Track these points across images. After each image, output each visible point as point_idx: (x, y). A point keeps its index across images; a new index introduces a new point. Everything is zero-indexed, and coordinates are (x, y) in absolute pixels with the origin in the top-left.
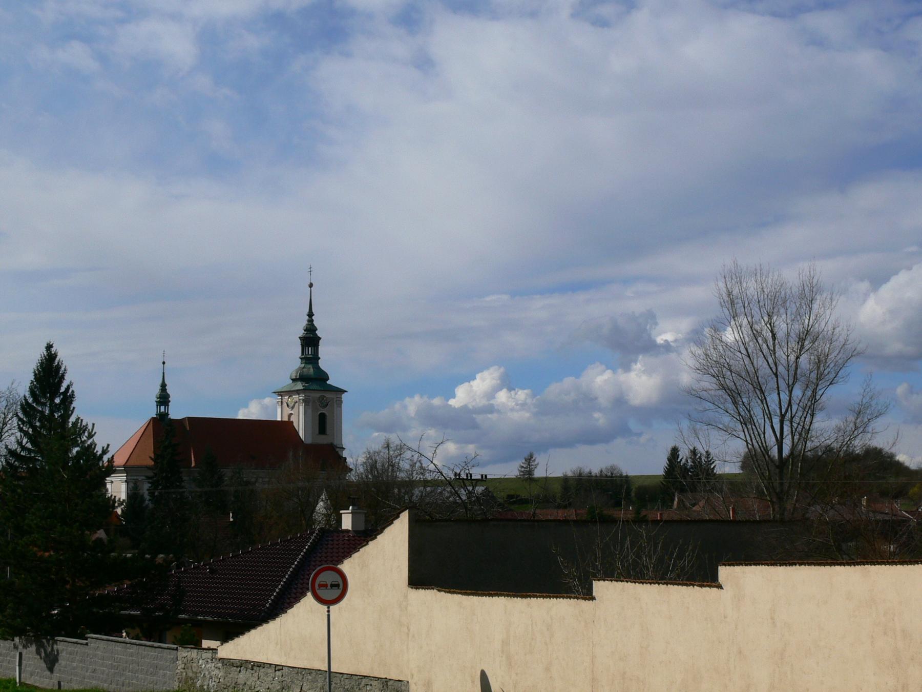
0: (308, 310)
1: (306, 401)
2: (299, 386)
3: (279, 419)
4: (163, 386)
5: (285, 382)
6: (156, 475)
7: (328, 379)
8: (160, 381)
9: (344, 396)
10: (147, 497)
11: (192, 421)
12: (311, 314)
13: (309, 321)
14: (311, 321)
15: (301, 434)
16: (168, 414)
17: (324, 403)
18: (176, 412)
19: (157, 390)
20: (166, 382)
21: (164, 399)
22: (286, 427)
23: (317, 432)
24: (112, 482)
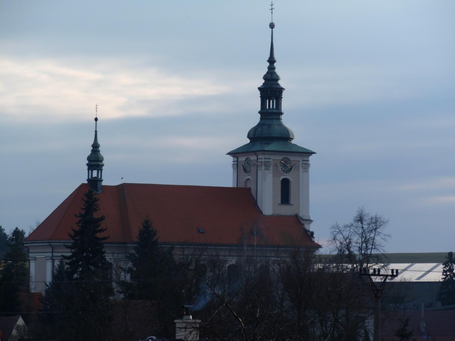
0: (268, 56)
4: (96, 147)
6: (74, 254)
9: (312, 158)
10: (255, 239)
11: (105, 186)
12: (272, 61)
14: (271, 69)
17: (287, 167)
18: (110, 179)
19: (88, 151)
20: (99, 141)
21: (95, 161)
24: (35, 259)
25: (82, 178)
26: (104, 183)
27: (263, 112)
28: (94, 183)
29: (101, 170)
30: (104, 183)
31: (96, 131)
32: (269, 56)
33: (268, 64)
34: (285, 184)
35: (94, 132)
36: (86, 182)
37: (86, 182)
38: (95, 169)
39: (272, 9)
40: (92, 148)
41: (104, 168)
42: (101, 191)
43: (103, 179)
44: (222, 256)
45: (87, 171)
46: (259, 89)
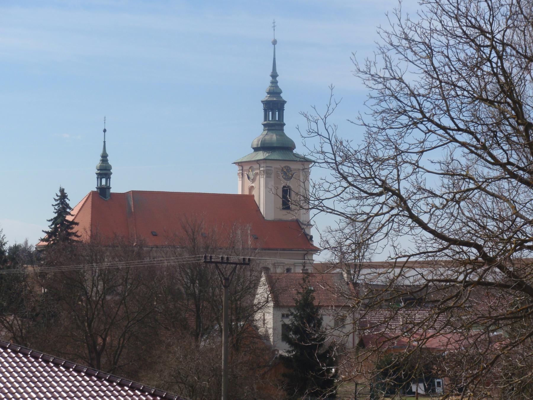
0: (271, 70)
1: (268, 174)
2: (261, 155)
3: (240, 193)
4: (104, 157)
5: (246, 153)
7: (294, 147)
8: (101, 152)
12: (274, 75)
13: (272, 82)
14: (274, 82)
15: (262, 210)
16: (109, 188)
17: (287, 174)
18: (119, 185)
19: (97, 161)
21: (104, 172)
22: (246, 202)
23: (280, 205)
25: (92, 185)
26: (112, 191)
28: (102, 192)
29: (110, 178)
30: (112, 191)
31: (104, 142)
32: (271, 71)
33: (271, 78)
34: (286, 191)
36: (96, 190)
37: (96, 190)
41: (112, 176)
42: (109, 198)
43: (111, 186)
46: (262, 102)
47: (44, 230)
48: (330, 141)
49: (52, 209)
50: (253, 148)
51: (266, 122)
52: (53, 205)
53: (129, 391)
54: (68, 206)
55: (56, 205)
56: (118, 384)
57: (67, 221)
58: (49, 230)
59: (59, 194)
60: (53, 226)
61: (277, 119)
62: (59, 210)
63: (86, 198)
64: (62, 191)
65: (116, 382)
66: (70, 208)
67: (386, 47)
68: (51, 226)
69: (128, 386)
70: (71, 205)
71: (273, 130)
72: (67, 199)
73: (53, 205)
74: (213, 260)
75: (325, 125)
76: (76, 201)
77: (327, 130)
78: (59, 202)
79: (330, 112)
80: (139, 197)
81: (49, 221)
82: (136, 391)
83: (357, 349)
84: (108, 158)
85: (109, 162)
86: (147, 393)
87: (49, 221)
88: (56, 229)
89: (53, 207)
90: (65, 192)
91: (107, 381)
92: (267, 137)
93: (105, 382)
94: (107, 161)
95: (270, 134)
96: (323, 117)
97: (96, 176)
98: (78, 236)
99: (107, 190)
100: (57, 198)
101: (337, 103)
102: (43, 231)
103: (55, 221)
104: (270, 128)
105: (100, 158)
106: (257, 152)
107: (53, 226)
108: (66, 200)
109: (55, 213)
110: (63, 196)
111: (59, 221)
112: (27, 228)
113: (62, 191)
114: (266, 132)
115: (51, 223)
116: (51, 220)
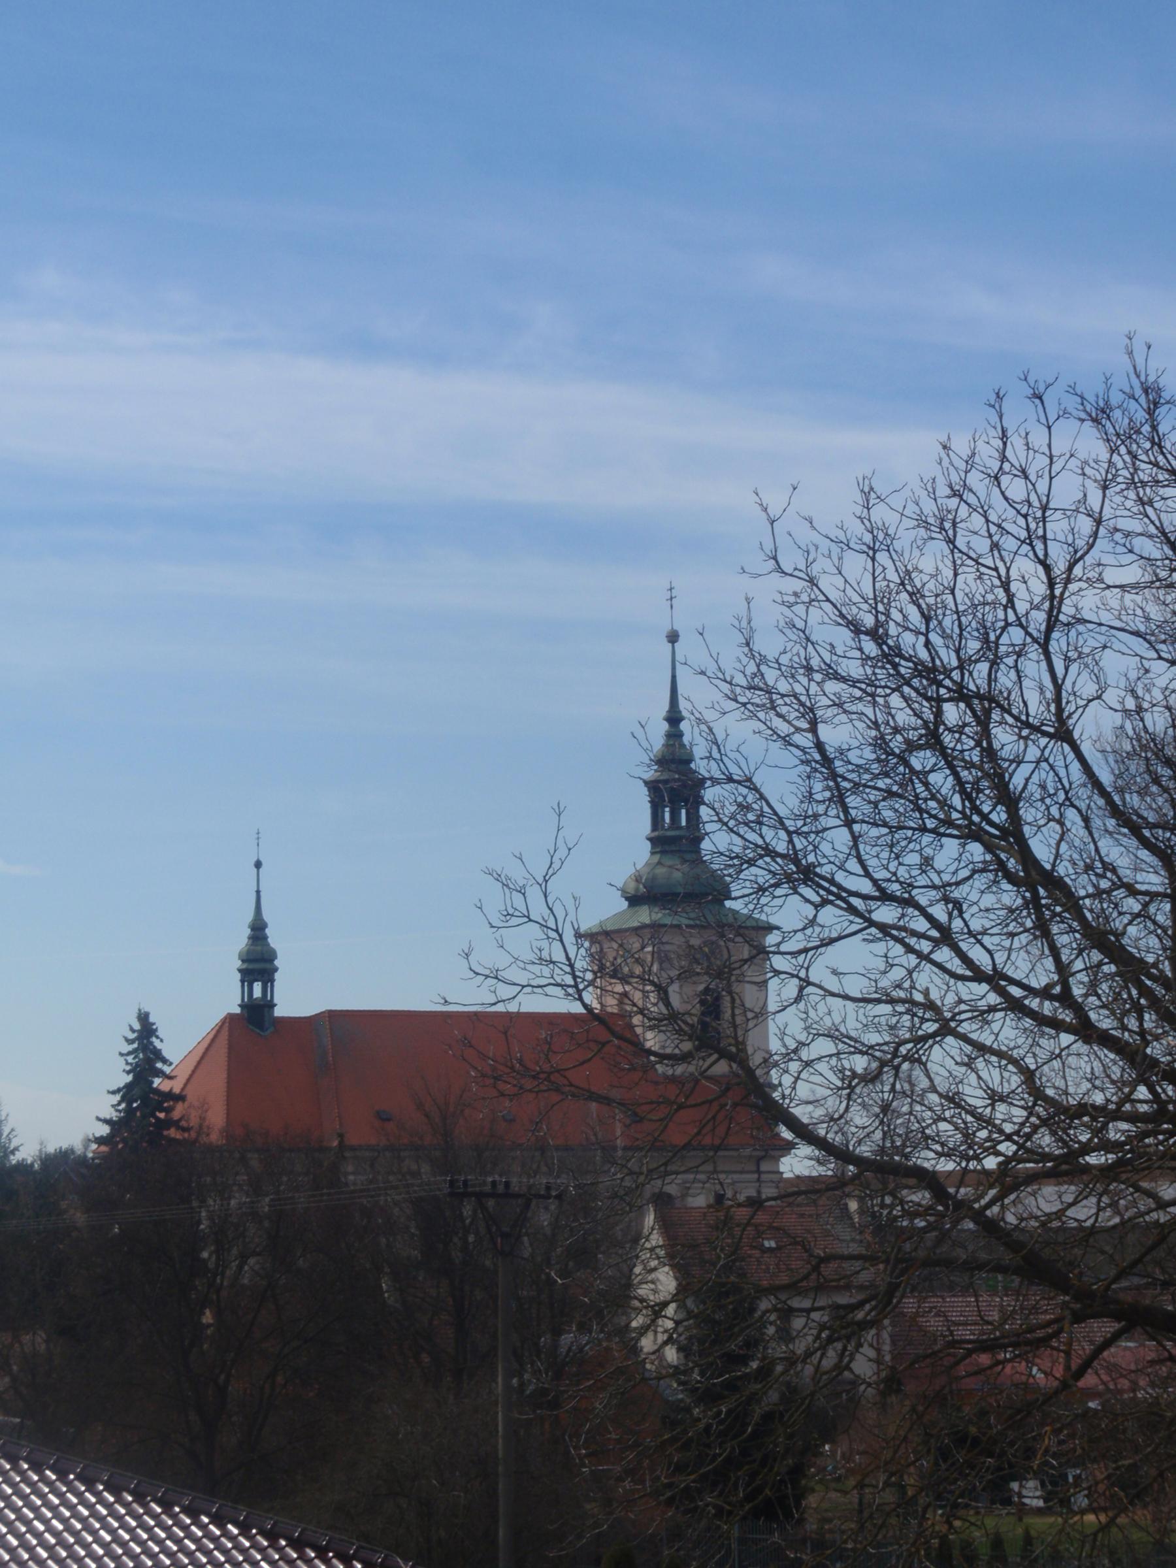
0: (665, 706)
2: (644, 915)
4: (258, 929)
14: (674, 735)
16: (271, 1006)
18: (294, 998)
19: (241, 939)
20: (267, 916)
21: (258, 964)
25: (229, 999)
26: (279, 1012)
27: (661, 842)
28: (256, 1015)
29: (272, 981)
30: (279, 1012)
31: (258, 892)
32: (667, 707)
33: (665, 726)
35: (254, 894)
36: (238, 1010)
37: (238, 1010)
38: (257, 980)
39: (671, 599)
40: (248, 931)
41: (277, 976)
42: (272, 1029)
43: (275, 1001)
44: (586, 1344)
45: (239, 984)
47: (102, 1116)
48: (560, 936)
49: (121, 1064)
50: (627, 899)
51: (656, 833)
52: (121, 1054)
53: (211, 1527)
54: (158, 1055)
55: (129, 1053)
56: (185, 1510)
57: (157, 1091)
58: (112, 1114)
59: (137, 1026)
60: (123, 1106)
61: (684, 823)
62: (137, 1065)
63: (213, 1033)
64: (143, 1018)
65: (179, 1506)
66: (165, 1061)
67: (716, 706)
68: (119, 1104)
69: (207, 1515)
70: (165, 1054)
71: (672, 852)
72: (157, 1037)
73: (121, 1054)
74: (470, 1190)
75: (546, 897)
76: (179, 1044)
77: (551, 909)
78: (135, 1045)
79: (556, 866)
80: (340, 1025)
81: (113, 1093)
82: (230, 1526)
83: (883, 1394)
84: (267, 931)
85: (269, 940)
86: (254, 1531)
87: (113, 1093)
88: (129, 1111)
89: (122, 1059)
90: (152, 1019)
91: (159, 1502)
92: (661, 871)
93: (153, 1505)
94: (265, 938)
95: (668, 861)
96: (541, 880)
97: (238, 976)
98: (184, 1130)
99: (266, 1009)
100: (132, 1036)
101: (570, 846)
102: (98, 1119)
103: (126, 1093)
104: (667, 848)
105: (248, 932)
106: (637, 908)
107: (123, 1106)
108: (154, 1039)
109: (128, 1072)
110: (146, 1031)
111: (136, 1091)
112: (61, 1110)
113: (143, 1018)
114: (657, 858)
115: (118, 1097)
116: (119, 1090)
